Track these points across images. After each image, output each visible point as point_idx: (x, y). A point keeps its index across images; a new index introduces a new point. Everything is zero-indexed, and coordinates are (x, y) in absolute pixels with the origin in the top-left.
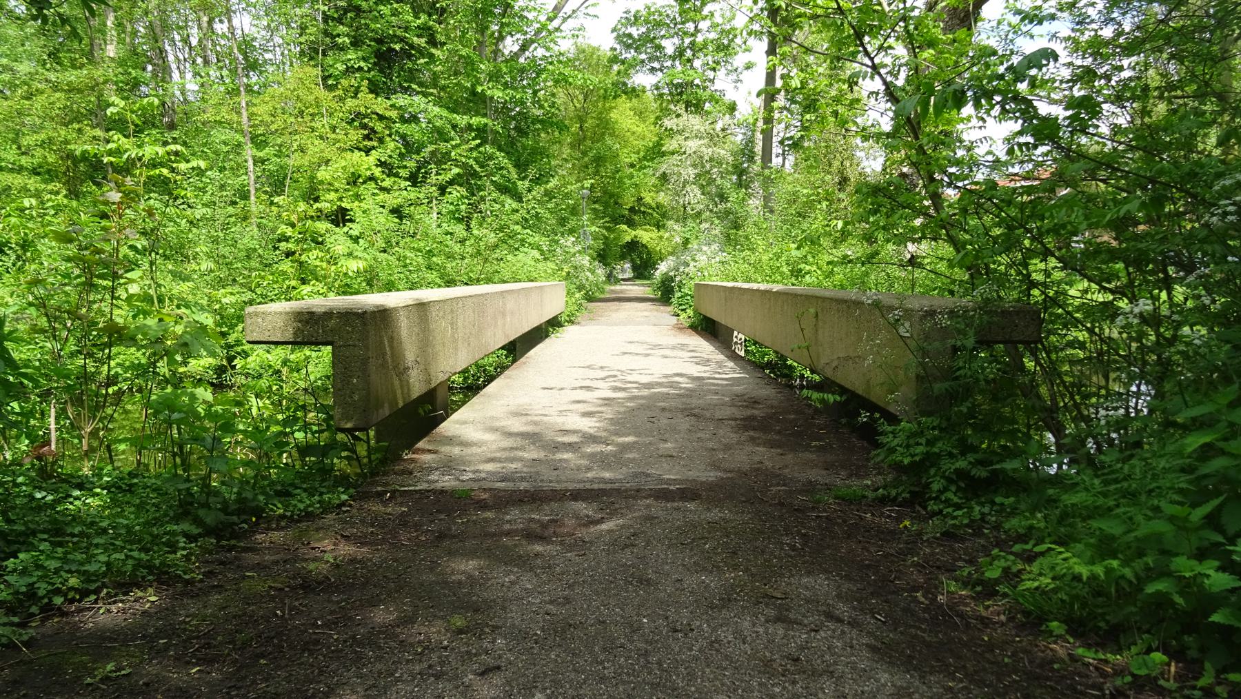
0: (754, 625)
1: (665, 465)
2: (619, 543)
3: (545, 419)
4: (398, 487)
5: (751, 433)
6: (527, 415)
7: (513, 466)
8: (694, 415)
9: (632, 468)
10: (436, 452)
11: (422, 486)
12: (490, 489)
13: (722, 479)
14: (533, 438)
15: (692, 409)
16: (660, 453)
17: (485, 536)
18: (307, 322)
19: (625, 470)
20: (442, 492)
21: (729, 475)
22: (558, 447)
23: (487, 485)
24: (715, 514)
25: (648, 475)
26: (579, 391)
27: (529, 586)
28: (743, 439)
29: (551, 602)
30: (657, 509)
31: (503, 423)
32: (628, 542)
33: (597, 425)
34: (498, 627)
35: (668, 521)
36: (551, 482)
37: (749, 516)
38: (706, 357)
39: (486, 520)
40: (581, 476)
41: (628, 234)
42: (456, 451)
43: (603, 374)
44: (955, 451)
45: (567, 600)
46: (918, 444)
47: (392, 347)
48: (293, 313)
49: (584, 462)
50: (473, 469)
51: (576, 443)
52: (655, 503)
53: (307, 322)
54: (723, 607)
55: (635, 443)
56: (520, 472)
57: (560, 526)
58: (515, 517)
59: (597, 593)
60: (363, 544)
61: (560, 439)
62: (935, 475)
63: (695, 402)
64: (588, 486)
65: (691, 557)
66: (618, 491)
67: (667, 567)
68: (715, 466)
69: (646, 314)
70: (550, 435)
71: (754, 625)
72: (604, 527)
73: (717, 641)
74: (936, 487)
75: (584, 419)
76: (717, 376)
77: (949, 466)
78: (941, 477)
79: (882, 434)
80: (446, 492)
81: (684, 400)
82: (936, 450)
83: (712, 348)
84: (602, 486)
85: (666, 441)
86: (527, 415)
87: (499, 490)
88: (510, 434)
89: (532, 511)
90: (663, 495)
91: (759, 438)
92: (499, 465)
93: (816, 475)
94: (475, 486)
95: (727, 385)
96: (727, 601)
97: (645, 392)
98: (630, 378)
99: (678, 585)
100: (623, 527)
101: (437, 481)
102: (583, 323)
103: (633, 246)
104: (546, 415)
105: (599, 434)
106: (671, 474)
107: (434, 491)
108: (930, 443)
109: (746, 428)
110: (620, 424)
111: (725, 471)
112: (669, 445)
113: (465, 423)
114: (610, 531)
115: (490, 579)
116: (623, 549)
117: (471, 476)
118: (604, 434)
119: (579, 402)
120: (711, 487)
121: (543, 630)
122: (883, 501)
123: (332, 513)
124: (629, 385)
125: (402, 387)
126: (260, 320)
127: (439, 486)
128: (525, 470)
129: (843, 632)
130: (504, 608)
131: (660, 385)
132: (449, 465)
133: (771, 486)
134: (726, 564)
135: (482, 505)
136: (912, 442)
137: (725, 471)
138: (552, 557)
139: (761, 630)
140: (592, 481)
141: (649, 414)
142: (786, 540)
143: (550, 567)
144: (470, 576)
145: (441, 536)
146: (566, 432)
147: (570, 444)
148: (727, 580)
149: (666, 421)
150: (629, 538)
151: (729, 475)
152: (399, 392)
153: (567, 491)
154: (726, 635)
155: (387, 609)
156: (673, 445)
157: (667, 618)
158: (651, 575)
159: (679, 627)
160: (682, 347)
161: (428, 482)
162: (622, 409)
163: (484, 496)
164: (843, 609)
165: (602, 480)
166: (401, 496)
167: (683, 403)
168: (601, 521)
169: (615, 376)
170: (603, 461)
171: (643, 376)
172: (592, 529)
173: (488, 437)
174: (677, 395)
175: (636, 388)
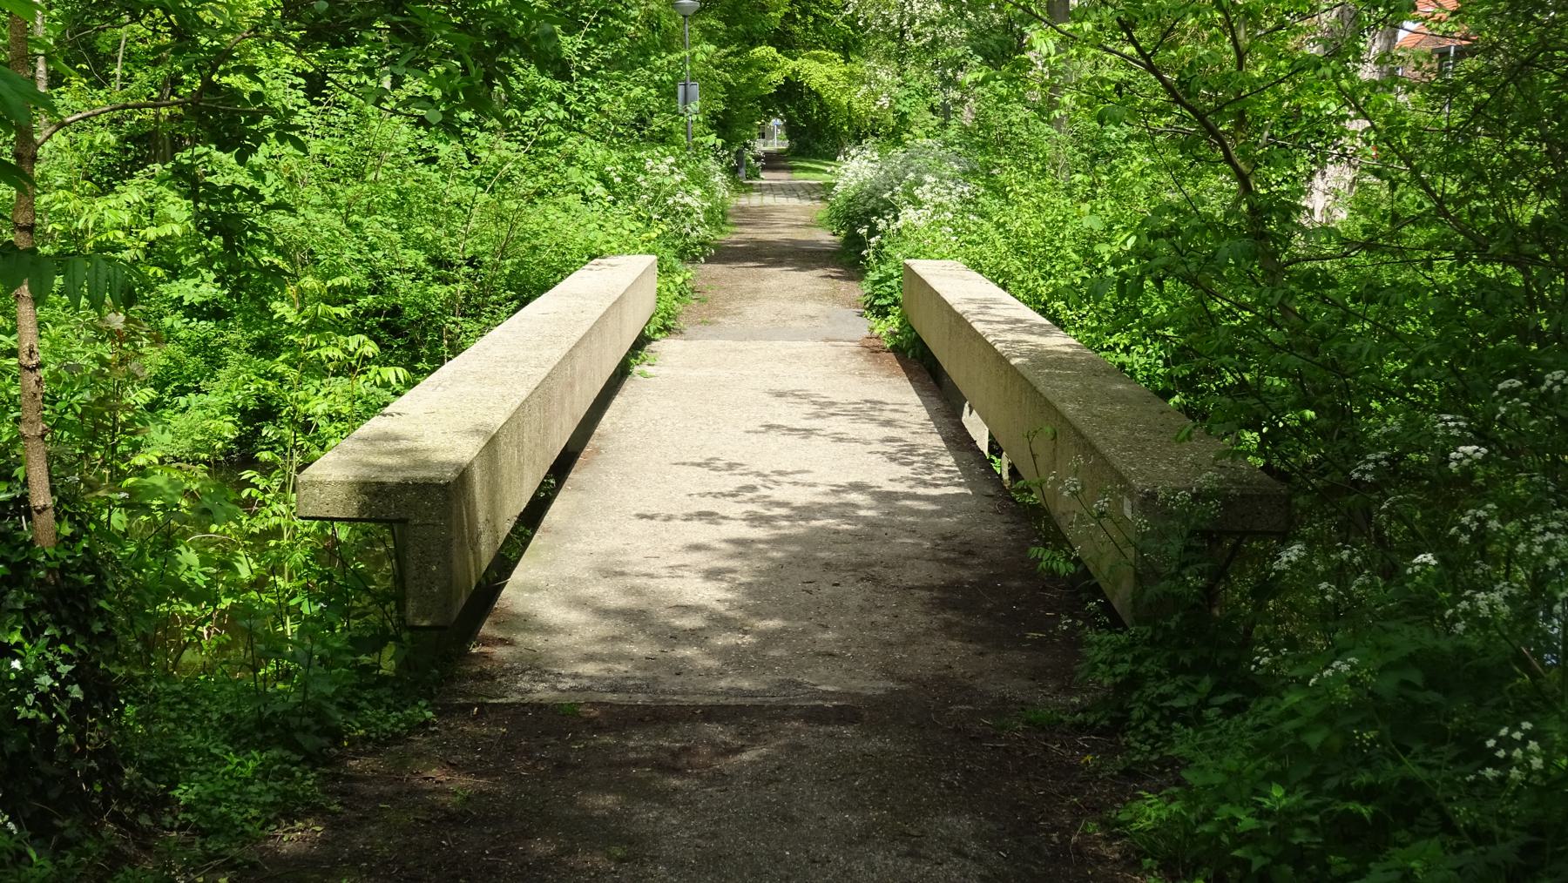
0: (886, 858)
1: (821, 669)
2: (762, 777)
3: (652, 582)
4: (485, 699)
5: (948, 615)
6: (622, 574)
7: (622, 668)
8: (872, 579)
9: (779, 674)
10: (511, 643)
11: (515, 698)
12: (600, 704)
13: (893, 691)
14: (636, 618)
15: (870, 565)
16: (817, 648)
17: (610, 765)
18: (376, 495)
19: (768, 677)
20: (540, 707)
21: (904, 686)
22: (677, 637)
23: (597, 697)
24: (874, 744)
25: (799, 685)
26: (696, 524)
27: (674, 822)
28: (935, 626)
29: (700, 837)
30: (806, 735)
31: (591, 591)
32: (772, 776)
33: (729, 596)
34: (656, 857)
35: (818, 753)
36: (675, 693)
37: (913, 746)
38: (910, 439)
39: (606, 745)
40: (712, 686)
41: (778, 66)
42: (538, 641)
43: (731, 482)
44: (1164, 672)
45: (714, 835)
46: (1124, 661)
47: (468, 515)
48: (358, 483)
49: (712, 663)
50: (569, 672)
51: (701, 629)
52: (805, 727)
53: (376, 495)
54: (860, 843)
55: (784, 630)
56: (634, 678)
57: (694, 756)
58: (639, 742)
59: (742, 829)
60: (479, 775)
61: (678, 623)
62: (1137, 700)
63: (878, 551)
64: (722, 701)
65: (837, 795)
66: (759, 707)
67: (812, 805)
68: (889, 674)
69: (811, 307)
70: (662, 615)
71: (886, 858)
72: (745, 757)
73: (850, 870)
74: (1136, 714)
75: (709, 584)
76: (921, 491)
77: (1152, 689)
78: (1144, 703)
79: (1090, 644)
80: (546, 706)
81: (860, 545)
82: (1142, 670)
83: (924, 414)
84: (740, 701)
85: (826, 627)
86: (622, 574)
87: (611, 704)
88: (605, 613)
89: (658, 735)
90: (816, 716)
91: (957, 624)
92: (603, 666)
93: (1015, 688)
94: (581, 698)
95: (933, 513)
96: (865, 837)
97: (801, 528)
98: (778, 494)
99: (821, 823)
100: (766, 758)
101: (530, 691)
102: (689, 330)
103: (792, 91)
104: (651, 576)
105: (731, 614)
106: (827, 682)
107: (531, 705)
108: (1138, 660)
109: (943, 605)
110: (760, 596)
111: (901, 680)
112: (829, 635)
113: (534, 589)
114: (752, 763)
115: (633, 815)
116: (767, 785)
117: (571, 683)
118: (738, 614)
119: (697, 548)
120: (878, 705)
121: (696, 859)
122: (1080, 728)
123: (418, 733)
124: (777, 511)
125: (475, 560)
126: (317, 491)
127: (536, 697)
128: (638, 674)
129: (964, 866)
130: (656, 842)
131: (825, 510)
132: (537, 666)
133: (951, 704)
134: (872, 803)
135: (596, 727)
136: (1118, 657)
137: (901, 680)
138: (692, 792)
139: (891, 862)
140: (727, 693)
141: (806, 574)
142: (945, 777)
143: (691, 803)
144: (612, 812)
145: (561, 766)
146: (686, 609)
147: (693, 631)
148: (870, 819)
149: (828, 590)
150: (773, 772)
151: (904, 686)
152: (473, 569)
153: (697, 707)
154: (859, 866)
155: (543, 841)
156: (836, 635)
157: (808, 851)
158: (795, 812)
159: (817, 859)
160: (868, 410)
161: (519, 691)
162: (765, 565)
163: (595, 713)
164: (973, 847)
165: (740, 692)
166: (491, 712)
167: (859, 553)
168: (741, 750)
169: (753, 488)
170: (736, 659)
171: (799, 489)
172: (732, 759)
173: (575, 616)
174: (851, 533)
175: (787, 518)
